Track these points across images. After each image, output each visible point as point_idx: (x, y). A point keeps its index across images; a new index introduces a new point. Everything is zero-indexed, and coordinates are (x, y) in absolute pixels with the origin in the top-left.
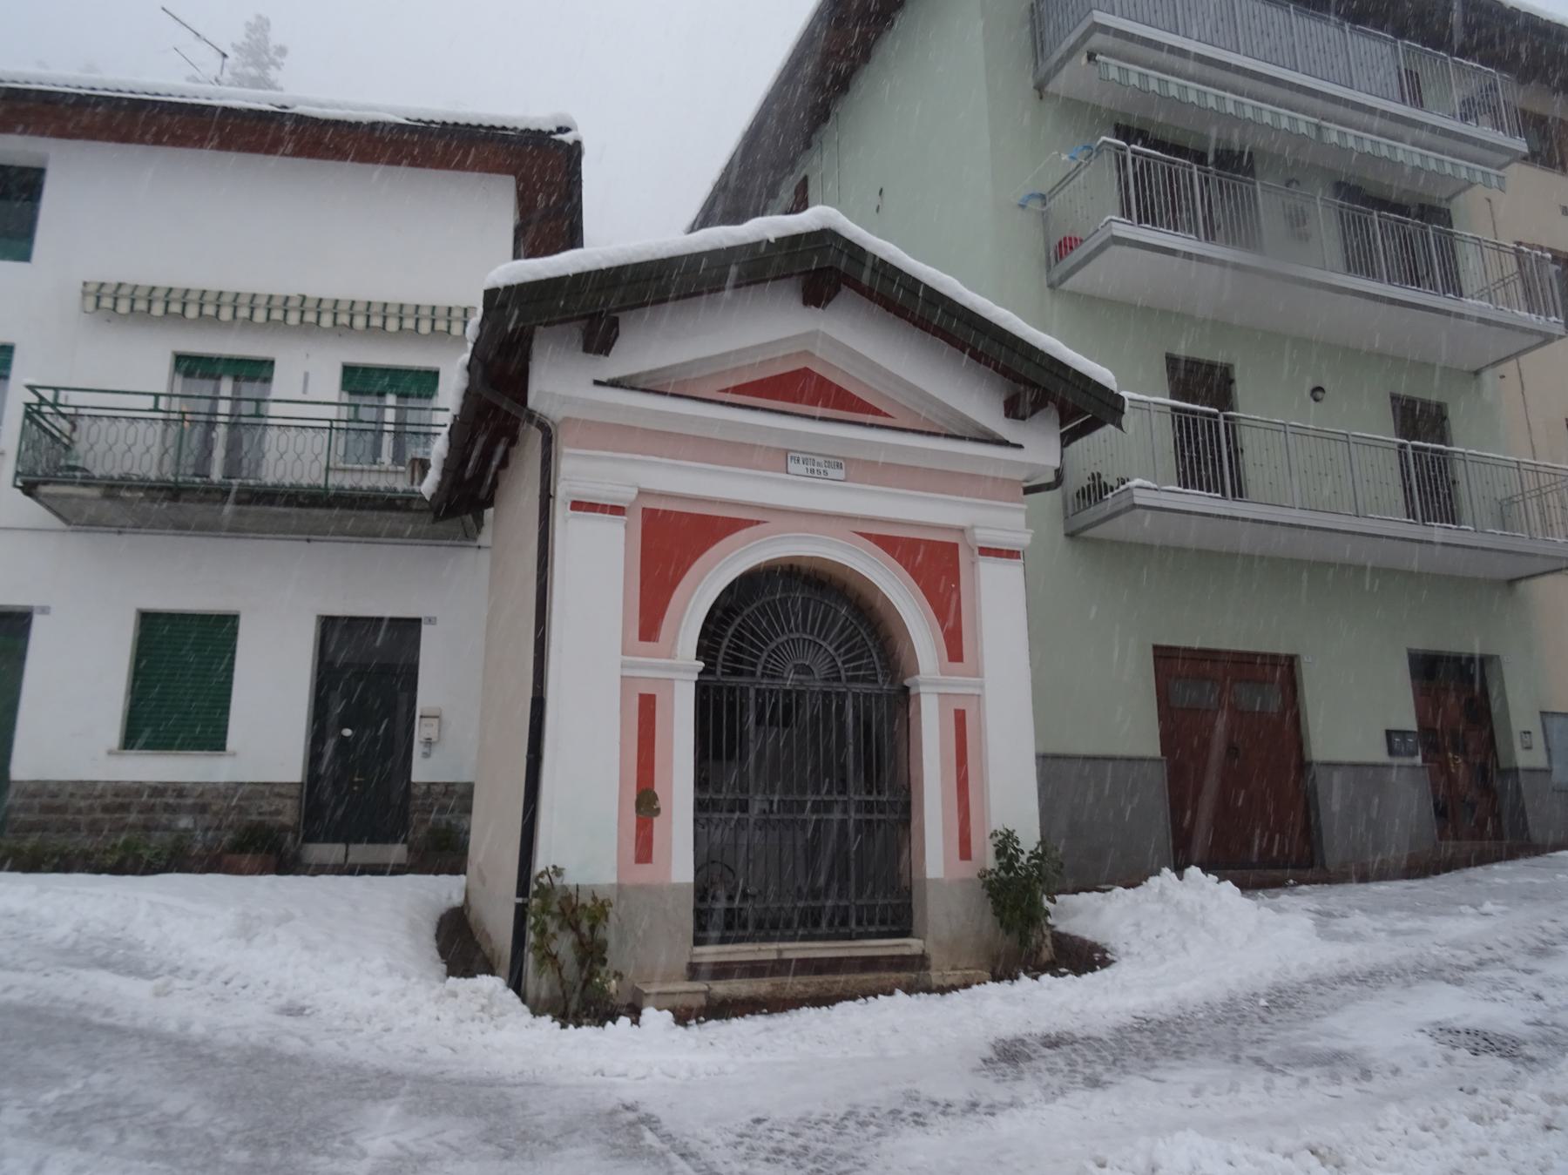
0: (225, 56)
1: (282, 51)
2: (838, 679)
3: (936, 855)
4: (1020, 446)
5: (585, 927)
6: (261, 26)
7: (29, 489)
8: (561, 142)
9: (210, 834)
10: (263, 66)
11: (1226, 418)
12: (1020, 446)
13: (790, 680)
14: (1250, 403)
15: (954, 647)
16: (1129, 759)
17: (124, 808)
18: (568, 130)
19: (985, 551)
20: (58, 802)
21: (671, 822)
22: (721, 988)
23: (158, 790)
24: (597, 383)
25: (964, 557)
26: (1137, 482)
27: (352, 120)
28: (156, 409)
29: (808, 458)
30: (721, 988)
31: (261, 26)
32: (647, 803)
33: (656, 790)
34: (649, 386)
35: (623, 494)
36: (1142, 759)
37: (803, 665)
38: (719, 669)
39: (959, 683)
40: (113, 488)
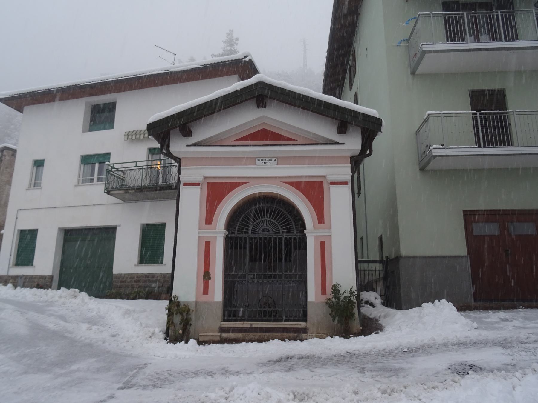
0: (175, 55)
1: (237, 39)
2: (279, 233)
3: (313, 293)
4: (344, 144)
5: (185, 314)
6: (231, 33)
7: (108, 193)
8: (245, 61)
9: (160, 288)
10: (231, 45)
11: (480, 114)
12: (344, 144)
13: (261, 235)
14: (514, 105)
15: (321, 218)
16: (451, 257)
17: (139, 281)
18: (247, 56)
19: (333, 183)
20: (124, 279)
21: (214, 281)
22: (225, 335)
23: (147, 276)
24: (187, 146)
25: (325, 186)
26: (434, 146)
27: (185, 70)
28: (136, 166)
29: (263, 159)
30: (225, 335)
31: (231, 33)
32: (207, 275)
33: (210, 272)
34: (208, 144)
35: (199, 179)
36: (462, 257)
37: (265, 228)
38: (236, 232)
39: (322, 232)
40: (140, 189)
